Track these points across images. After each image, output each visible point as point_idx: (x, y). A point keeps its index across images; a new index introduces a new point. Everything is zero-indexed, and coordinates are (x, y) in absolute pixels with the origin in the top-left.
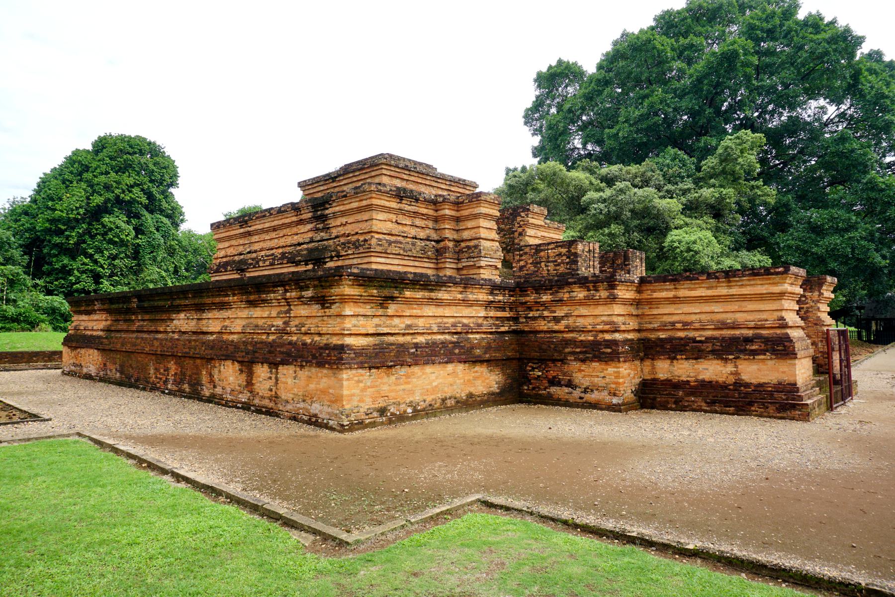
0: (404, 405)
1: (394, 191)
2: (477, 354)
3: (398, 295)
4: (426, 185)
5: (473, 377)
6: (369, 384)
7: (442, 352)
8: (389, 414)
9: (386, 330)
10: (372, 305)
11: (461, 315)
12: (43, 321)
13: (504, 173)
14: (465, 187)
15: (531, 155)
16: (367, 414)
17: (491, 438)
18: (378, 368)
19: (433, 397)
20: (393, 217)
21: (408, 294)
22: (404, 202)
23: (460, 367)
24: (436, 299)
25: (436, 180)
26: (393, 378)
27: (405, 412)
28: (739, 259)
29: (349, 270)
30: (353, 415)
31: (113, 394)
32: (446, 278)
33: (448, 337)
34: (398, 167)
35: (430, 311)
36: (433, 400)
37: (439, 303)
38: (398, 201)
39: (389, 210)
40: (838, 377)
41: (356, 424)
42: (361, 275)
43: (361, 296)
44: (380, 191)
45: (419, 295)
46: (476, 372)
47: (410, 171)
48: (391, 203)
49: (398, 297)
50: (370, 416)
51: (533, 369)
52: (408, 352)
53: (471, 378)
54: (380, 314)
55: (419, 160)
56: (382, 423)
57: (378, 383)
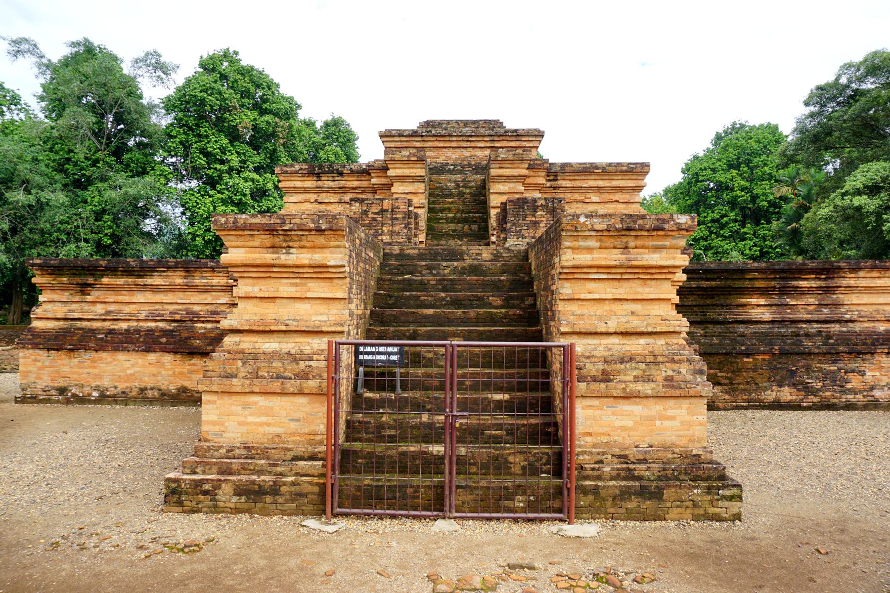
0: (89, 388)
1: (305, 169)
2: (195, 345)
3: (92, 282)
4: (453, 148)
5: (188, 370)
6: (47, 363)
7: (142, 340)
8: (69, 394)
9: (76, 315)
10: (71, 292)
11: (188, 302)
14: (520, 138)
18: (58, 350)
19: (128, 385)
20: (313, 197)
21: (105, 280)
22: (323, 178)
23: (168, 358)
24: (145, 285)
25: (465, 139)
26: (75, 361)
27: (90, 395)
29: (31, 262)
30: (29, 389)
32: (152, 263)
33: (162, 325)
34: (403, 136)
35: (140, 297)
36: (127, 388)
37: (155, 289)
38: (315, 178)
39: (306, 190)
41: (29, 398)
42: (45, 265)
43: (50, 283)
44: (286, 172)
45: (120, 281)
46: (194, 365)
47: (422, 136)
48: (306, 182)
49: (94, 284)
50: (48, 393)
52: (95, 337)
53: (186, 371)
54: (77, 300)
55: (474, 119)
56: (58, 402)
57: (56, 364)
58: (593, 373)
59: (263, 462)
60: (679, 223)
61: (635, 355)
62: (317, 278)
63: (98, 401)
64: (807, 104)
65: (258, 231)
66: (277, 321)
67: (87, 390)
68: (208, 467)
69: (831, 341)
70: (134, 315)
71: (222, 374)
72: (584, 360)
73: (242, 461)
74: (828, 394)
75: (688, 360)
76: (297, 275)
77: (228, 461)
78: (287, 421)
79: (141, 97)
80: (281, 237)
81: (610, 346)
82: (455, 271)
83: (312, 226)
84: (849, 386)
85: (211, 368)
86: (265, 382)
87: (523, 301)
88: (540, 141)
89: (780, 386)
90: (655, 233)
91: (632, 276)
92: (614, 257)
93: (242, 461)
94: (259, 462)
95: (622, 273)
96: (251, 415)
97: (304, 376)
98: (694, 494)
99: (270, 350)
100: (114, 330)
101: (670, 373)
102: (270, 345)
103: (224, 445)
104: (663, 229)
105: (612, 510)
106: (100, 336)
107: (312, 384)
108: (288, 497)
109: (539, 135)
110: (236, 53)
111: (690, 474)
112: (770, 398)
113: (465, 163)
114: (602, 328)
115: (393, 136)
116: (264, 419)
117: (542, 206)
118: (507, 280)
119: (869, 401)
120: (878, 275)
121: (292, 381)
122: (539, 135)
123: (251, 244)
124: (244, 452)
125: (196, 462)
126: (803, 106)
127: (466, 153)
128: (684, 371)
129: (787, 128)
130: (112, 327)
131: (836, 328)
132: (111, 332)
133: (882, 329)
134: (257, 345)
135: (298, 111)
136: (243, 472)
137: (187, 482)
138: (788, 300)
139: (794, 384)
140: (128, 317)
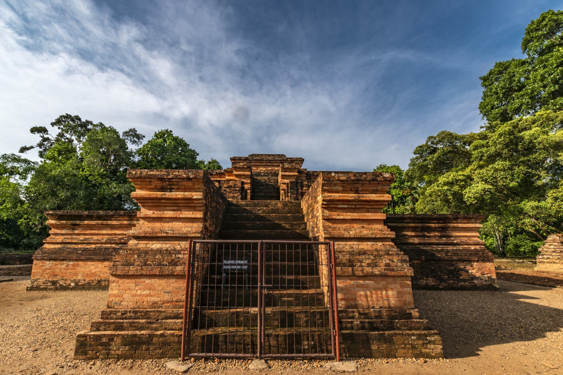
8: (58, 285)
16: (44, 283)
17: (529, 303)
21: (86, 222)
36: (91, 280)
37: (113, 227)
40: (438, 332)
50: (46, 284)
56: (50, 289)
58: (344, 261)
59: (144, 321)
60: (385, 177)
61: (367, 250)
62: (187, 206)
63: (73, 289)
64: (415, 153)
65: (154, 179)
66: (161, 231)
67: (68, 282)
68: (107, 326)
69: (449, 254)
70: (100, 240)
71: (124, 263)
72: (338, 253)
73: (130, 321)
74: (451, 282)
75: (397, 254)
76: (175, 205)
77: (122, 321)
78: (162, 293)
79: (127, 149)
80: (167, 183)
81: (352, 246)
82: (264, 212)
83: (185, 176)
84: (461, 278)
85: (118, 260)
86: (150, 268)
87: (299, 226)
88: (302, 163)
89: (427, 277)
90: (372, 182)
91: (361, 206)
92: (351, 196)
93: (130, 321)
94: (141, 321)
95: (355, 205)
96: (140, 289)
97: (174, 263)
98: (412, 340)
99: (156, 248)
100: (88, 248)
101: (388, 261)
102: (156, 245)
103: (121, 310)
104: (377, 180)
105: (363, 351)
106: (80, 252)
107: (179, 269)
108: (157, 346)
109: (302, 160)
110: (171, 131)
111: (407, 326)
112: (423, 283)
113: (269, 172)
114: (346, 235)
115: (237, 160)
116: (147, 292)
117: (306, 185)
118: (291, 216)
119: (472, 286)
120: (466, 222)
121: (167, 267)
122: (302, 160)
123: (149, 187)
124: (132, 314)
125: (100, 322)
126: (413, 154)
128: (395, 260)
129: (405, 167)
130: (87, 247)
131: (450, 248)
132: (85, 250)
133: (473, 248)
134: (148, 246)
135: (197, 156)
136: (130, 328)
137: (92, 337)
138: (426, 233)
139: (434, 276)
140: (96, 242)
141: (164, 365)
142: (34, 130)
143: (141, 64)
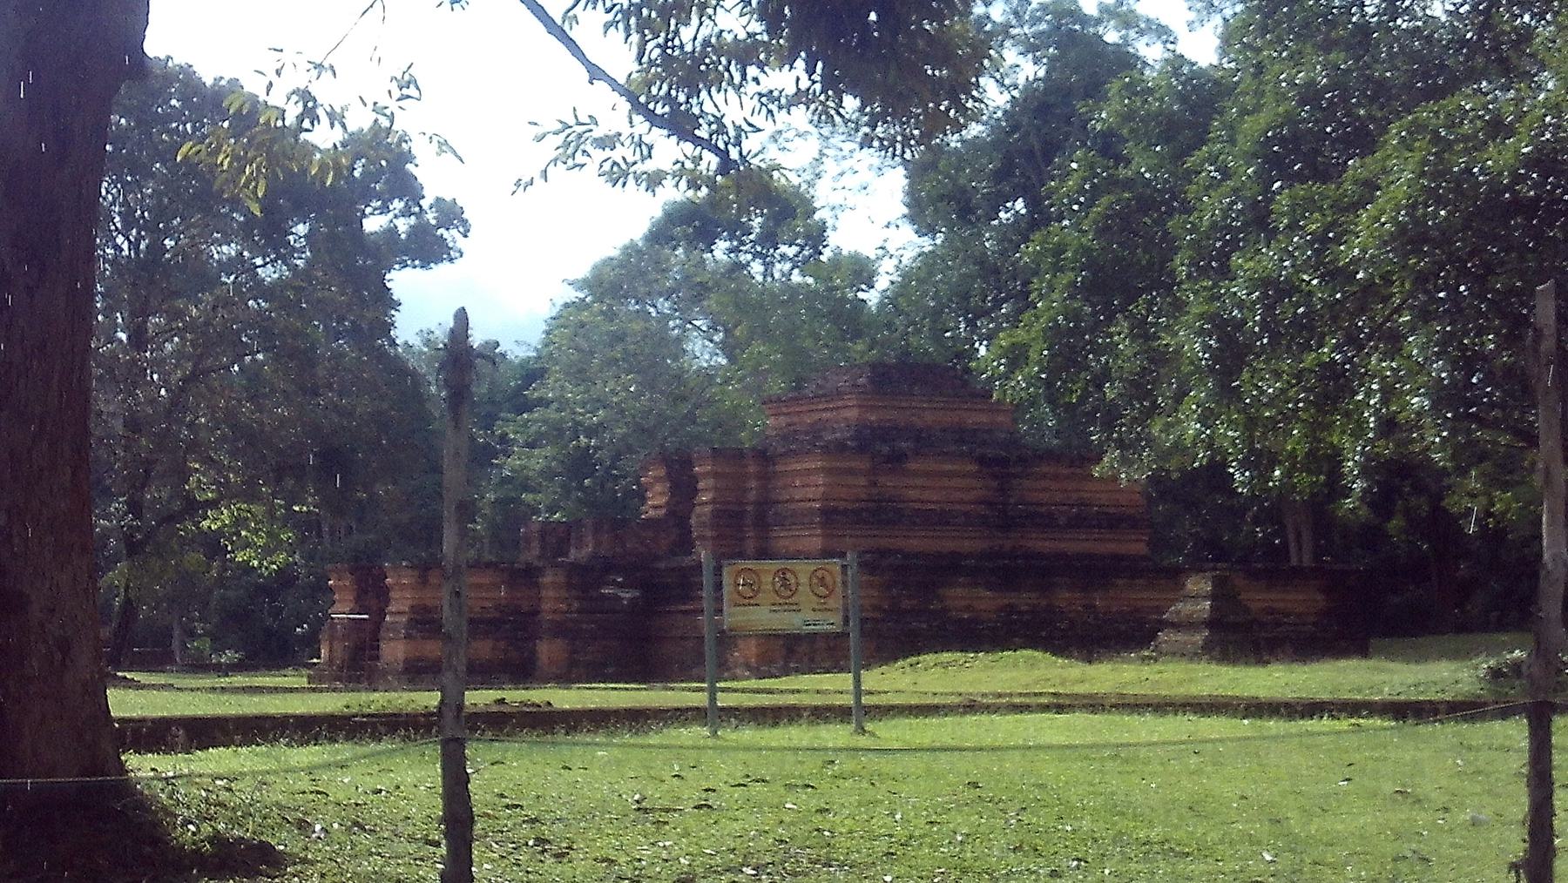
12: (749, 464)
13: (517, 180)
15: (440, 196)
28: (747, 650)
31: (1117, 712)
51: (1501, 507)
109: (1005, 60)
127: (816, 416)
141: (1503, 219)
142: (592, 84)
143: (581, 289)
